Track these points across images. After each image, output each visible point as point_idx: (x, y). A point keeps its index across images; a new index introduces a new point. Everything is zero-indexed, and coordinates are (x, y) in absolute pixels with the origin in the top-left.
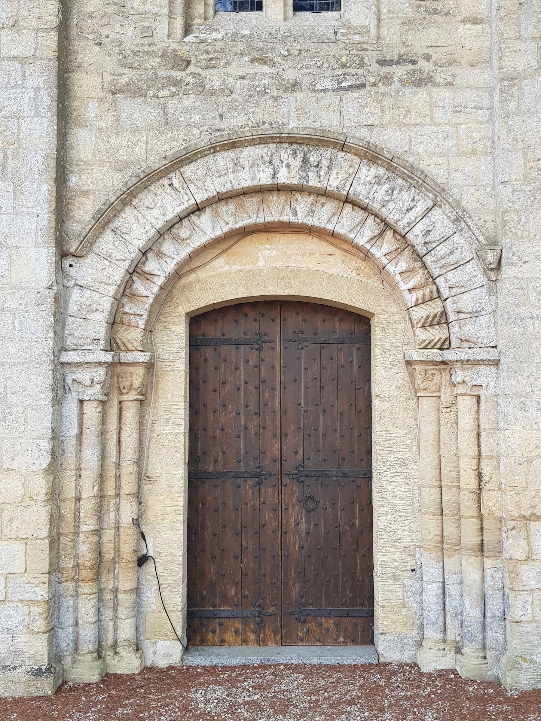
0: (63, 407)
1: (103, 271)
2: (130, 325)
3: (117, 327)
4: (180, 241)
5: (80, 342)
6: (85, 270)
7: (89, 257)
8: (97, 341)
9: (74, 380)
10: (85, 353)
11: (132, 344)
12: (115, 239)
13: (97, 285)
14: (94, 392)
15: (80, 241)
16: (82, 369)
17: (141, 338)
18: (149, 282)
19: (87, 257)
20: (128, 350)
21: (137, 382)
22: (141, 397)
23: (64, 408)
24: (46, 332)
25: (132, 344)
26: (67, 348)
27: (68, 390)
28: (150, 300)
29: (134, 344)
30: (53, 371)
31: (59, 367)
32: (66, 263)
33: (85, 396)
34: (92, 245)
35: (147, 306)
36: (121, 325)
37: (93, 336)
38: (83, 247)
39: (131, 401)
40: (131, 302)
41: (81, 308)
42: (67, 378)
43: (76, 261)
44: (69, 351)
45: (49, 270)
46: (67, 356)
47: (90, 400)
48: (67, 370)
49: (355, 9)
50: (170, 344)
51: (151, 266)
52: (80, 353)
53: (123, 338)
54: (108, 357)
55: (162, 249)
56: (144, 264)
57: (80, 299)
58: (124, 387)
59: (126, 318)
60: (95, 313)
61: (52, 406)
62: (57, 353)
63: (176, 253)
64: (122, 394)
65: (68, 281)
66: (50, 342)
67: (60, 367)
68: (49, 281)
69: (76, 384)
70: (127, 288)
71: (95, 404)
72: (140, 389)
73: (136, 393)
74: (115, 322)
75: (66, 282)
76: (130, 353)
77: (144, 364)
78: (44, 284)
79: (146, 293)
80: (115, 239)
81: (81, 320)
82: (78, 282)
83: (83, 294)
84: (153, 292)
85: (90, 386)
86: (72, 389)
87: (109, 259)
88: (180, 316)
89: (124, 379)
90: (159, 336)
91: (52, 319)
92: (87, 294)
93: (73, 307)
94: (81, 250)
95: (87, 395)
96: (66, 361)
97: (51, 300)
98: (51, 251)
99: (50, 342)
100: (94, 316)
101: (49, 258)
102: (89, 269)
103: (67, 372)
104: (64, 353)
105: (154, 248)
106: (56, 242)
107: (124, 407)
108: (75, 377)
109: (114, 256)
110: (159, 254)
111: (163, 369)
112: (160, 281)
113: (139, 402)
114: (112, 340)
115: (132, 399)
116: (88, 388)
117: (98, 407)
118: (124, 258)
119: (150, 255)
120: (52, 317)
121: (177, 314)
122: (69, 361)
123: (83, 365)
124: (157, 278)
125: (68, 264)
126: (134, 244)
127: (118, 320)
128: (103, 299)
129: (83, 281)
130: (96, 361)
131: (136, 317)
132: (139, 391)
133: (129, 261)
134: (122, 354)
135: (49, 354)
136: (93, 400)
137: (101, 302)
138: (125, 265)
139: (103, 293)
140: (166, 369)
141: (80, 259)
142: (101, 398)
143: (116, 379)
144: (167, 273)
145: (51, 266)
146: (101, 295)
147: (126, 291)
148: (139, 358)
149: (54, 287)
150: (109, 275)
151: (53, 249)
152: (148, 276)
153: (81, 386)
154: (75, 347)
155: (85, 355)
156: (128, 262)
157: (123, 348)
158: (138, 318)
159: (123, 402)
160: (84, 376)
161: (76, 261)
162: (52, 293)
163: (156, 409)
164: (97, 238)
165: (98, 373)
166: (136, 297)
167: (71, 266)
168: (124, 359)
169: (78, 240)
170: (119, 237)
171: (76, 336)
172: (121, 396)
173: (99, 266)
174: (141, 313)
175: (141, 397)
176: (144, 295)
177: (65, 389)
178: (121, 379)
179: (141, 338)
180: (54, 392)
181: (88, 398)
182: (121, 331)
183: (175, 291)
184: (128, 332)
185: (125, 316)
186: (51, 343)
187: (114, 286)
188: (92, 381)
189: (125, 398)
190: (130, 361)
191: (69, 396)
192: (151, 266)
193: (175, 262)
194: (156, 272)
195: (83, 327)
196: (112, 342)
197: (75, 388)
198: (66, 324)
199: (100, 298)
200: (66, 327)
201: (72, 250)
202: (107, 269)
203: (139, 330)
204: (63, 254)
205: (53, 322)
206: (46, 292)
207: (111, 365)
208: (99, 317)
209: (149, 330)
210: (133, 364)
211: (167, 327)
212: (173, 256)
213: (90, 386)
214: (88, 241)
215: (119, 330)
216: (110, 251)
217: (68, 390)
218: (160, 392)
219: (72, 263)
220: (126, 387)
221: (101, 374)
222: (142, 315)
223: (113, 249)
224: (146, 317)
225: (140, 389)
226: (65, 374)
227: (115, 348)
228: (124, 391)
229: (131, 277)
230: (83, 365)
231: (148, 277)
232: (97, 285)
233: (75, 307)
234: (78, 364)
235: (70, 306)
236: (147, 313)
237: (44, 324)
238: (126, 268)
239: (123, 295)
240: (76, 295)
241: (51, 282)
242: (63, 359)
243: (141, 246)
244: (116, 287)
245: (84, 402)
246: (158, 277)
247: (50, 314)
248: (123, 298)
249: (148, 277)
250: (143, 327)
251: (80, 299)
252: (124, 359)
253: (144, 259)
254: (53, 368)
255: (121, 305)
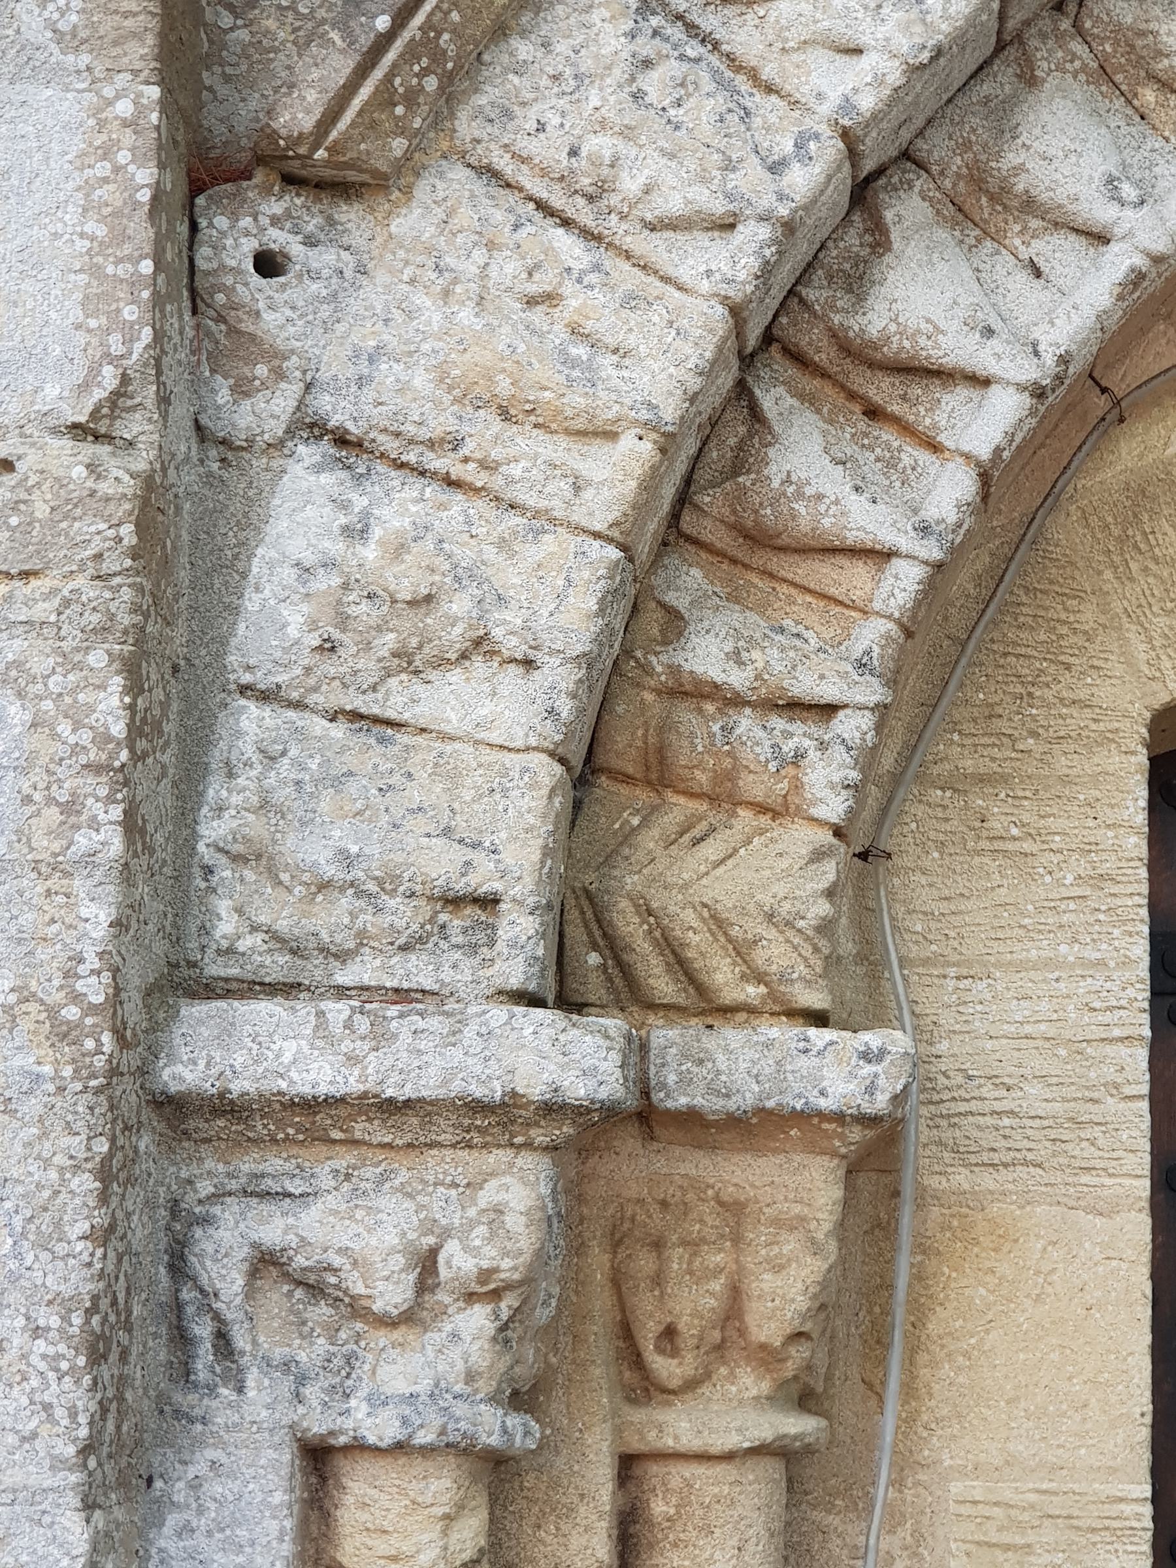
0: (163, 1505)
1: (537, 316)
2: (724, 795)
3: (619, 804)
4: (1149, 96)
5: (331, 919)
6: (395, 307)
7: (422, 190)
8: (471, 912)
9: (266, 1263)
10: (378, 1021)
11: (741, 950)
12: (646, 47)
13: (483, 432)
14: (427, 1378)
15: (365, 41)
16: (343, 1160)
17: (823, 908)
18: (888, 435)
19: (408, 191)
20: (713, 1009)
21: (785, 1287)
22: (797, 1425)
23: (173, 1520)
24: (53, 815)
25: (741, 950)
26: (215, 969)
27: (205, 1354)
28: (902, 583)
29: (759, 956)
30: (105, 1174)
31: (144, 1143)
32: (233, 237)
33: (358, 1406)
34: (450, 96)
35: (871, 635)
36: (643, 796)
37: (441, 865)
38: (385, 97)
39: (729, 1457)
40: (734, 598)
41: (343, 621)
42: (205, 1242)
43: (312, 224)
44: (228, 994)
45: (95, 271)
46: (227, 1032)
47: (400, 1448)
48: (208, 1171)
49: (782, 10)
50: (1020, 967)
51: (922, 294)
52: (337, 1011)
53: (669, 902)
54: (575, 1060)
55: (1012, 159)
56: (856, 282)
57: (336, 547)
58: (670, 1333)
59: (697, 734)
60: (455, 676)
61: (89, 1506)
62: (133, 1012)
63: (1128, 191)
64: (644, 1388)
65: (243, 389)
66: (87, 910)
67: (166, 1135)
68: (94, 371)
69: (276, 1298)
70: (703, 475)
71: (440, 1485)
72: (799, 1354)
73: (765, 1387)
74: (619, 754)
75: (223, 396)
76: (732, 1036)
77: (856, 1134)
78: (52, 391)
79: (866, 519)
80: (646, 47)
81: (338, 731)
82: (324, 403)
83: (360, 502)
84: (931, 513)
85: (408, 1318)
86: (241, 1341)
87: (584, 214)
88: (1107, 739)
89: (677, 1259)
90: (925, 898)
91: (110, 707)
92: (399, 505)
93: (274, 620)
94: (367, 122)
95: (378, 1401)
96: (209, 1088)
97: (107, 533)
98: (124, 108)
99: (87, 910)
100: (451, 700)
101: (103, 169)
102: (420, 299)
103: (205, 1188)
104: (194, 1011)
105: (938, 147)
106: (163, 36)
107: (659, 1508)
108: (274, 1228)
109: (630, 184)
110: (987, 207)
111: (961, 1178)
112: (985, 424)
113: (773, 1469)
114: (573, 915)
115: (733, 1441)
116: (382, 1338)
117: (461, 1507)
118: (719, 207)
119: (907, 210)
120: (117, 682)
121: (1078, 718)
122: (237, 1087)
123: (359, 1129)
124: (955, 399)
125: (249, 246)
126: (804, 92)
127: (624, 748)
128: (533, 553)
129: (369, 394)
130: (478, 1091)
131: (778, 723)
132: (790, 1369)
133: (764, 232)
134: (665, 1036)
135: (72, 1013)
136: (427, 1451)
137: (510, 577)
138: (732, 263)
139: (531, 500)
140: (988, 1181)
141: (349, 214)
142: (492, 1426)
143: (598, 1261)
144: (1049, 360)
145: (119, 237)
146: (515, 520)
147: (703, 514)
148: (815, 1079)
149: (137, 426)
150: (580, 351)
151: (138, 98)
152: (881, 387)
153: (322, 1311)
154: (277, 966)
155: (380, 1037)
156: (753, 237)
157: (664, 986)
158: (798, 735)
159: (654, 1468)
160: (357, 1223)
161: (312, 224)
162: (121, 476)
163: (905, 1533)
164: (500, 31)
165: (488, 1195)
166: (775, 562)
167: (268, 264)
168: (685, 1081)
169: (350, 38)
170: (676, 32)
171: (297, 871)
172: (638, 1415)
173: (507, 268)
174: (829, 692)
175: (797, 1425)
176: (852, 537)
177: (182, 1339)
178: (645, 1262)
179: (823, 908)
180: (105, 1372)
181: (381, 1428)
182: (649, 840)
183: (1066, 532)
184: (711, 850)
185: (685, 715)
186: (98, 915)
187: (627, 441)
188: (427, 1265)
189: (678, 1426)
190: (732, 1105)
191: (221, 1407)
192: (922, 294)
193: (1120, 261)
194: (956, 347)
195: (352, 787)
196: (576, 933)
197: (269, 1331)
198: (216, 757)
199: (503, 544)
200: (215, 790)
201: (298, 115)
202: (574, 300)
203: (801, 838)
204: (208, 163)
205: (118, 729)
206: (69, 461)
207: (585, 1137)
208: (486, 709)
209: (865, 851)
210: (761, 1127)
211: (996, 825)
212: (1102, 213)
213: (408, 1318)
214: (426, 46)
215: (628, 836)
216: (600, 145)
217: (205, 1354)
218: (944, 1381)
219: (278, 239)
220: (688, 1327)
221: (503, 1206)
222: (829, 710)
223: (627, 133)
224: (866, 721)
225: (799, 1354)
226: (189, 1201)
227: (595, 989)
228: (666, 1368)
229: (742, 389)
230: (359, 1129)
231: (880, 389)
232: (483, 432)
233: (295, 619)
234: (312, 1119)
235: (252, 603)
236: (872, 692)
237: (37, 740)
238: (735, 294)
239: (675, 534)
240: (302, 514)
241: (109, 378)
242: (185, 1072)
243: (867, 102)
244: (647, 448)
245: (343, 1464)
246: (962, 392)
247: (97, 658)
248: (672, 560)
249: (880, 389)
250: (834, 808)
251: (336, 547)
252: (685, 1081)
253: (852, 239)
254: (102, 1146)
255: (652, 622)
